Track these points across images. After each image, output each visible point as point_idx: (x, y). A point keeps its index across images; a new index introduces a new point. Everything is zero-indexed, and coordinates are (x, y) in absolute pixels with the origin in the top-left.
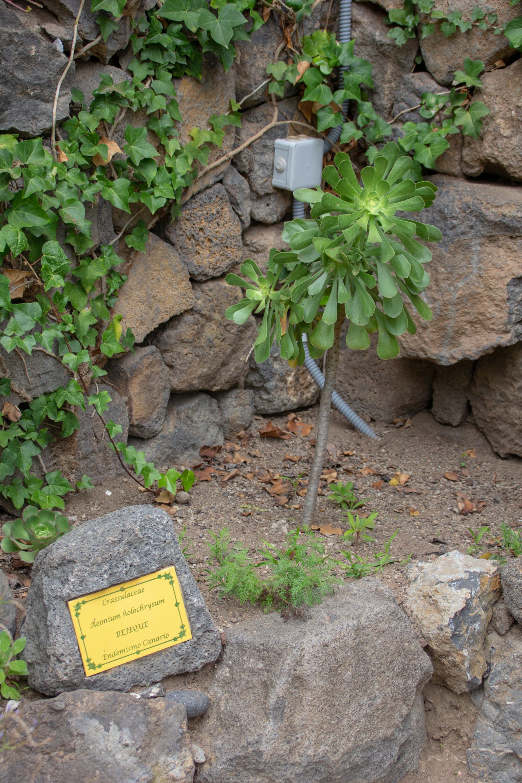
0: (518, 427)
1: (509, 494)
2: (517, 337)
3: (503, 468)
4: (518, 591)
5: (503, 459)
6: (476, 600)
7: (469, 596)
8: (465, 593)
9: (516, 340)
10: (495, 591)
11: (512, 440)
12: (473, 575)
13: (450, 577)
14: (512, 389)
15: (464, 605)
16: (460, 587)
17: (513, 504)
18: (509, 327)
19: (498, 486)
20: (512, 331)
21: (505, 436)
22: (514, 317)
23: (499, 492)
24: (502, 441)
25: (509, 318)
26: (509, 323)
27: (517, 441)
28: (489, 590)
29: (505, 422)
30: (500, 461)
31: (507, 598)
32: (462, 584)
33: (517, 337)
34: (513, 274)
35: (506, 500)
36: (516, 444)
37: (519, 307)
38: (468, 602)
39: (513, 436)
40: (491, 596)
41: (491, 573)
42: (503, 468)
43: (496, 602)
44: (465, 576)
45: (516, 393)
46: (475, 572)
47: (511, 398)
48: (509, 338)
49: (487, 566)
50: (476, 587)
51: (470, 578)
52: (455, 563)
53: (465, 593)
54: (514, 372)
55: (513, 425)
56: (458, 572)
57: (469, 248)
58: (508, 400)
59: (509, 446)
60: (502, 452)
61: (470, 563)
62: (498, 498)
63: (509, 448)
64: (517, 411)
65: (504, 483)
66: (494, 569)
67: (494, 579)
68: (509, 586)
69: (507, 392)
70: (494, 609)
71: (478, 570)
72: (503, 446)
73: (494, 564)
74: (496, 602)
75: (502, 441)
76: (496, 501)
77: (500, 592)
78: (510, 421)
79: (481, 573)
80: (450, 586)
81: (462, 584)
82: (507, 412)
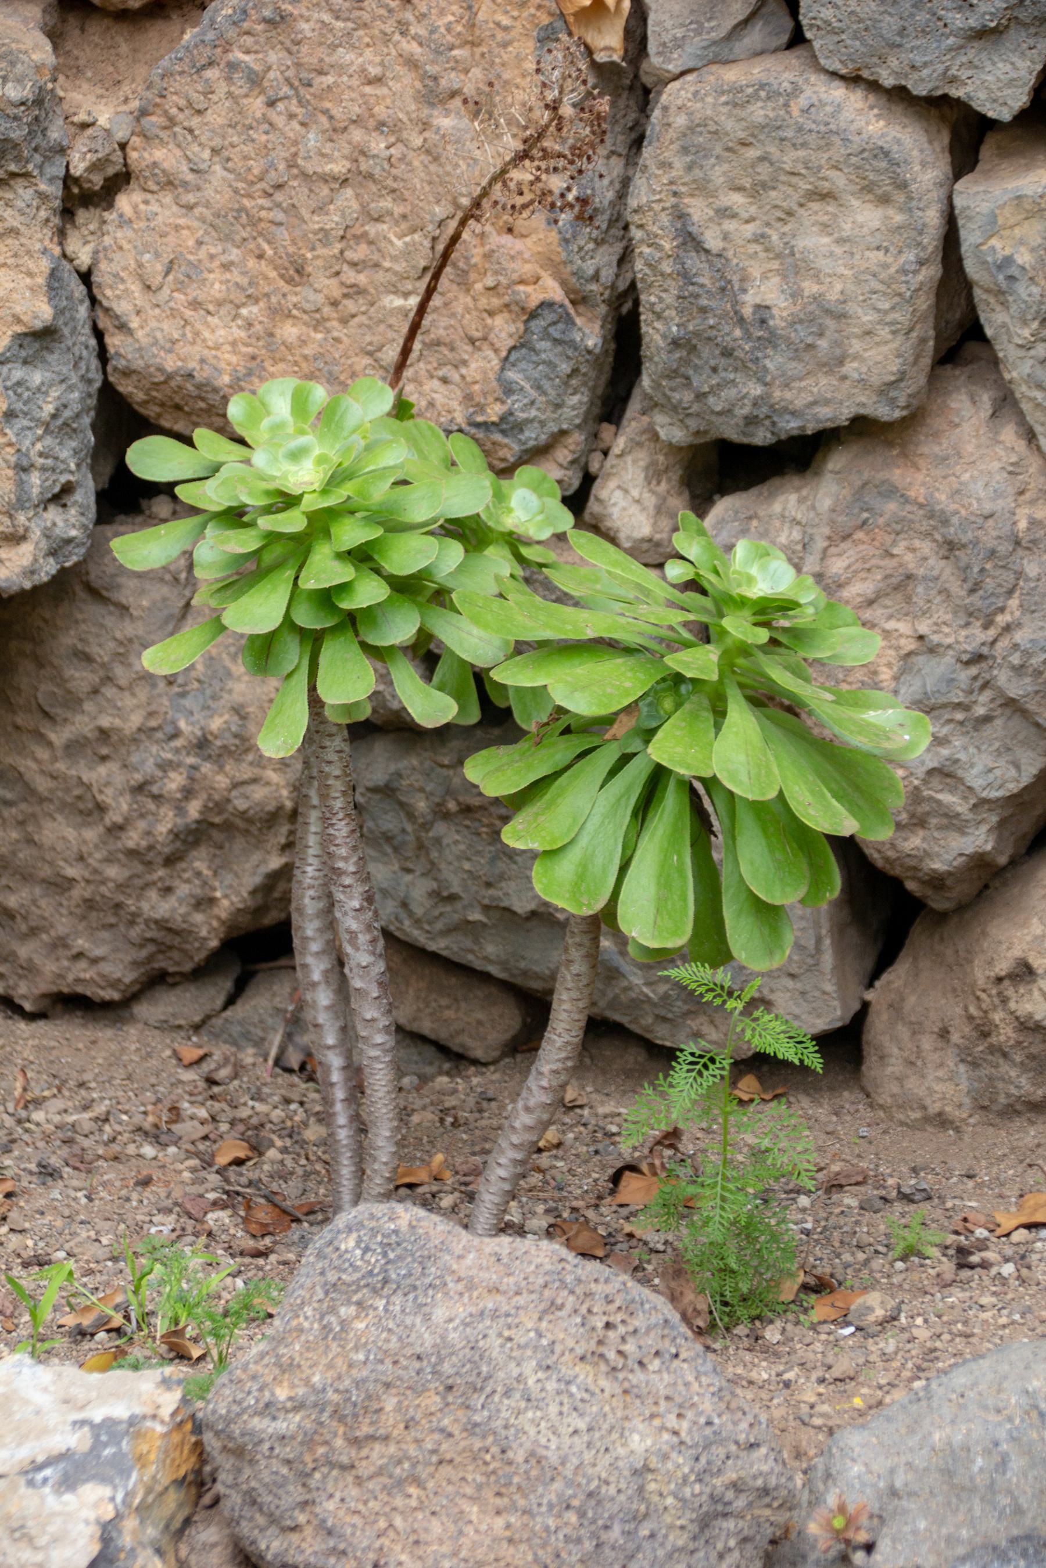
0: (78, 893)
1: (86, 1143)
2: (53, 553)
3: (38, 1048)
4: (275, 1465)
5: (31, 1017)
6: (130, 1524)
7: (109, 1513)
8: (92, 1502)
9: (49, 568)
10: (180, 1483)
11: (61, 943)
12: (106, 1431)
13: (24, 1453)
14: (43, 754)
15: (95, 1548)
16: (68, 1483)
17: (110, 1173)
18: (21, 518)
19: (38, 1116)
20: (36, 534)
21: (34, 932)
22: (35, 479)
23: (47, 1138)
24: (24, 951)
25: (20, 484)
26: (21, 503)
27: (81, 943)
28: (165, 1479)
29: (26, 877)
30: (22, 1027)
31: (234, 1500)
32: (72, 1470)
33: (53, 553)
34: (18, 320)
35: (83, 1164)
36: (79, 956)
37: (49, 441)
38: (108, 1532)
39: (63, 925)
40: (173, 1499)
41: (166, 1412)
42: (38, 1048)
43: (187, 1522)
44: (77, 1441)
45: (61, 766)
46: (109, 1423)
47: (42, 784)
48: (26, 561)
49: (146, 1394)
50: (125, 1473)
51: (97, 1445)
52: (26, 1402)
53: (92, 1502)
54: (45, 688)
55: (60, 885)
56: (45, 1431)
57: (758, 307)
58: (30, 793)
59: (49, 967)
60: (25, 993)
61: (79, 1393)
62: (55, 1161)
63: (53, 972)
64: (70, 833)
65: (59, 1104)
66: (170, 1401)
67: (176, 1438)
68: (239, 1452)
69: (26, 765)
70: (184, 1551)
71: (120, 1411)
72: (29, 970)
73: (166, 1383)
74: (187, 1522)
75: (24, 951)
76: (47, 1173)
77: (198, 1485)
78: (46, 871)
79: (133, 1421)
80: (31, 1483)
81: (72, 1470)
82: (30, 841)
